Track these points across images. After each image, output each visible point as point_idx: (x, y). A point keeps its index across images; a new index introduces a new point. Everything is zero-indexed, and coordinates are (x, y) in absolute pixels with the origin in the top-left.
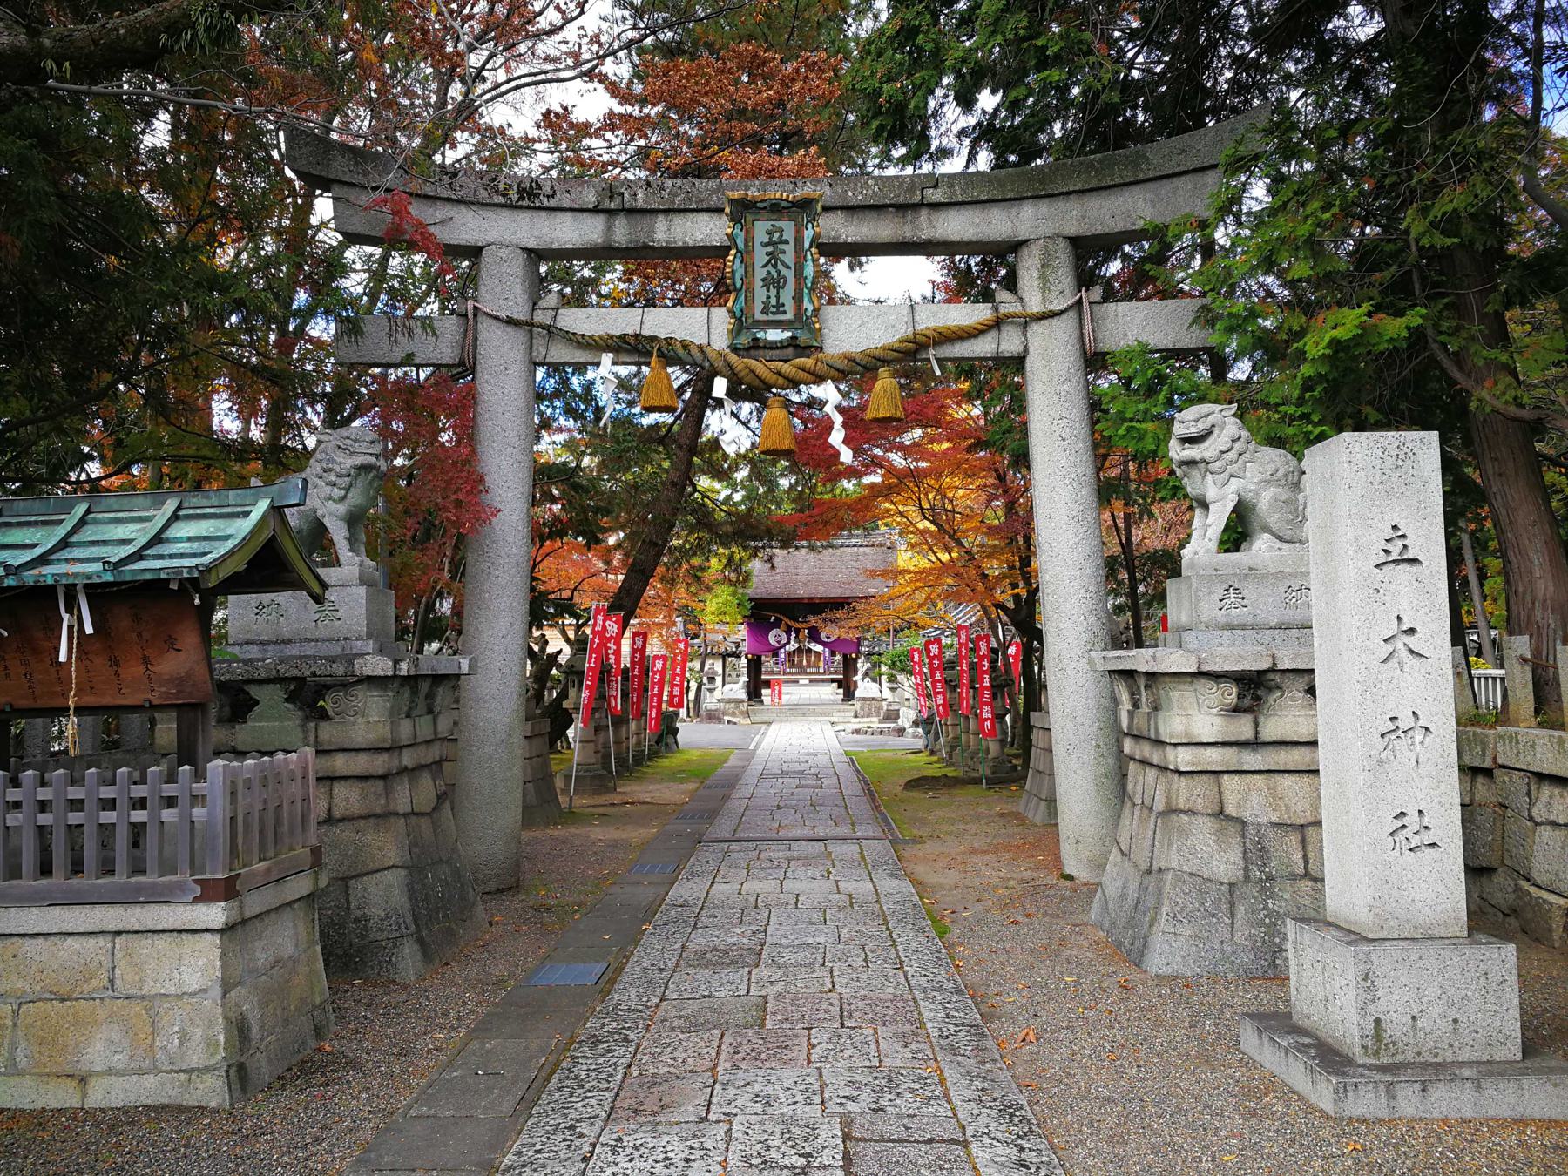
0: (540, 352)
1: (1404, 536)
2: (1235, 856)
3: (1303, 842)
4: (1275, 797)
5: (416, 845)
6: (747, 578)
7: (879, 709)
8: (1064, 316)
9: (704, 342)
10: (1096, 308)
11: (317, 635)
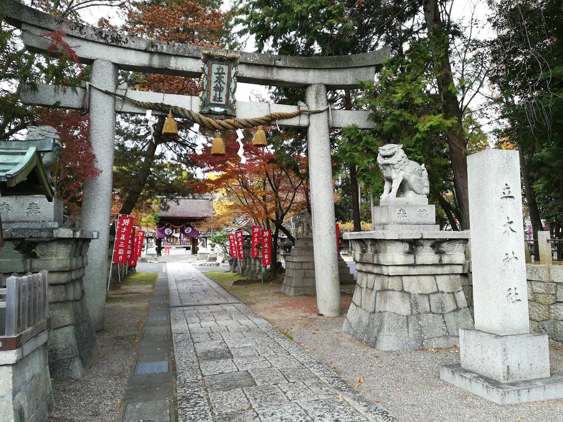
0: (119, 107)
1: (509, 188)
2: (408, 306)
3: (429, 300)
4: (420, 284)
5: (76, 314)
6: (169, 207)
7: (206, 257)
8: (323, 113)
9: (190, 109)
11: (28, 219)
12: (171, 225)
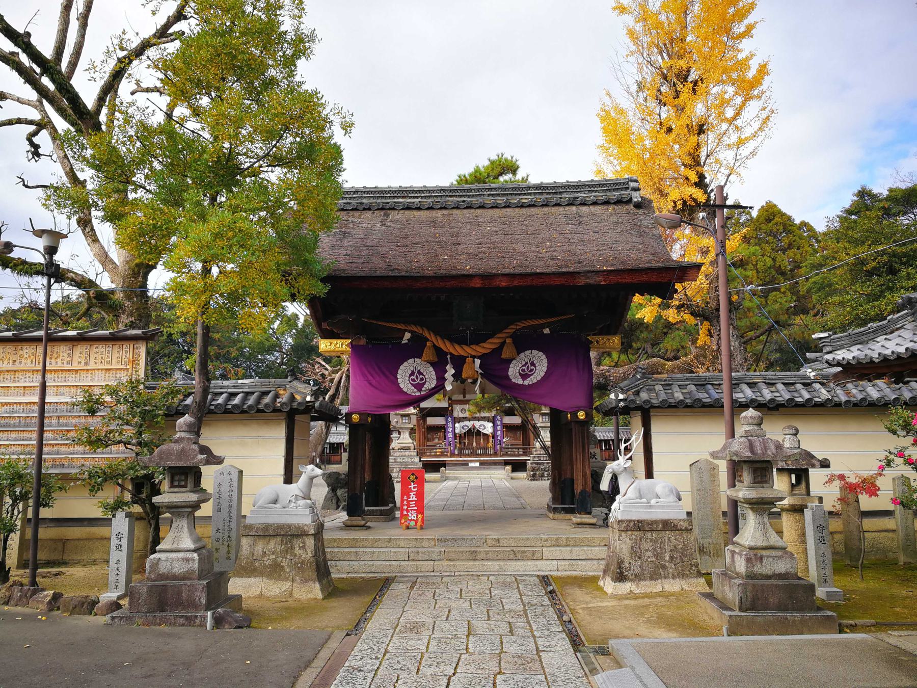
12: (433, 339)
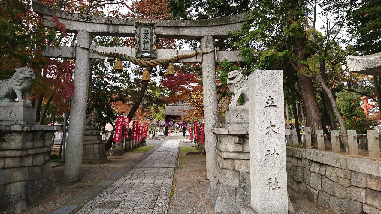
2: (237, 180)
8: (211, 53)
10: (218, 52)
11: (9, 119)
